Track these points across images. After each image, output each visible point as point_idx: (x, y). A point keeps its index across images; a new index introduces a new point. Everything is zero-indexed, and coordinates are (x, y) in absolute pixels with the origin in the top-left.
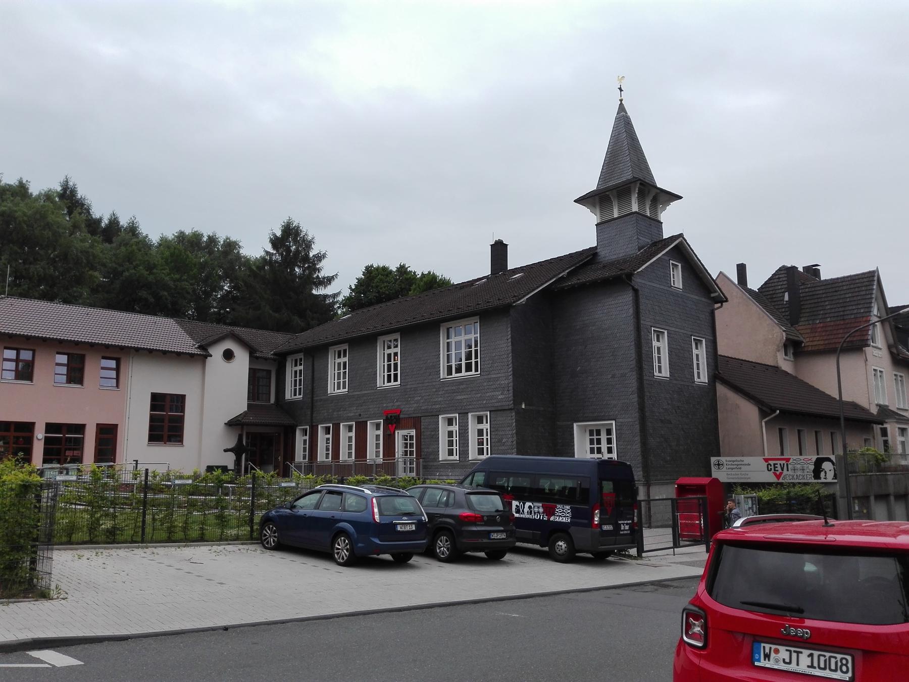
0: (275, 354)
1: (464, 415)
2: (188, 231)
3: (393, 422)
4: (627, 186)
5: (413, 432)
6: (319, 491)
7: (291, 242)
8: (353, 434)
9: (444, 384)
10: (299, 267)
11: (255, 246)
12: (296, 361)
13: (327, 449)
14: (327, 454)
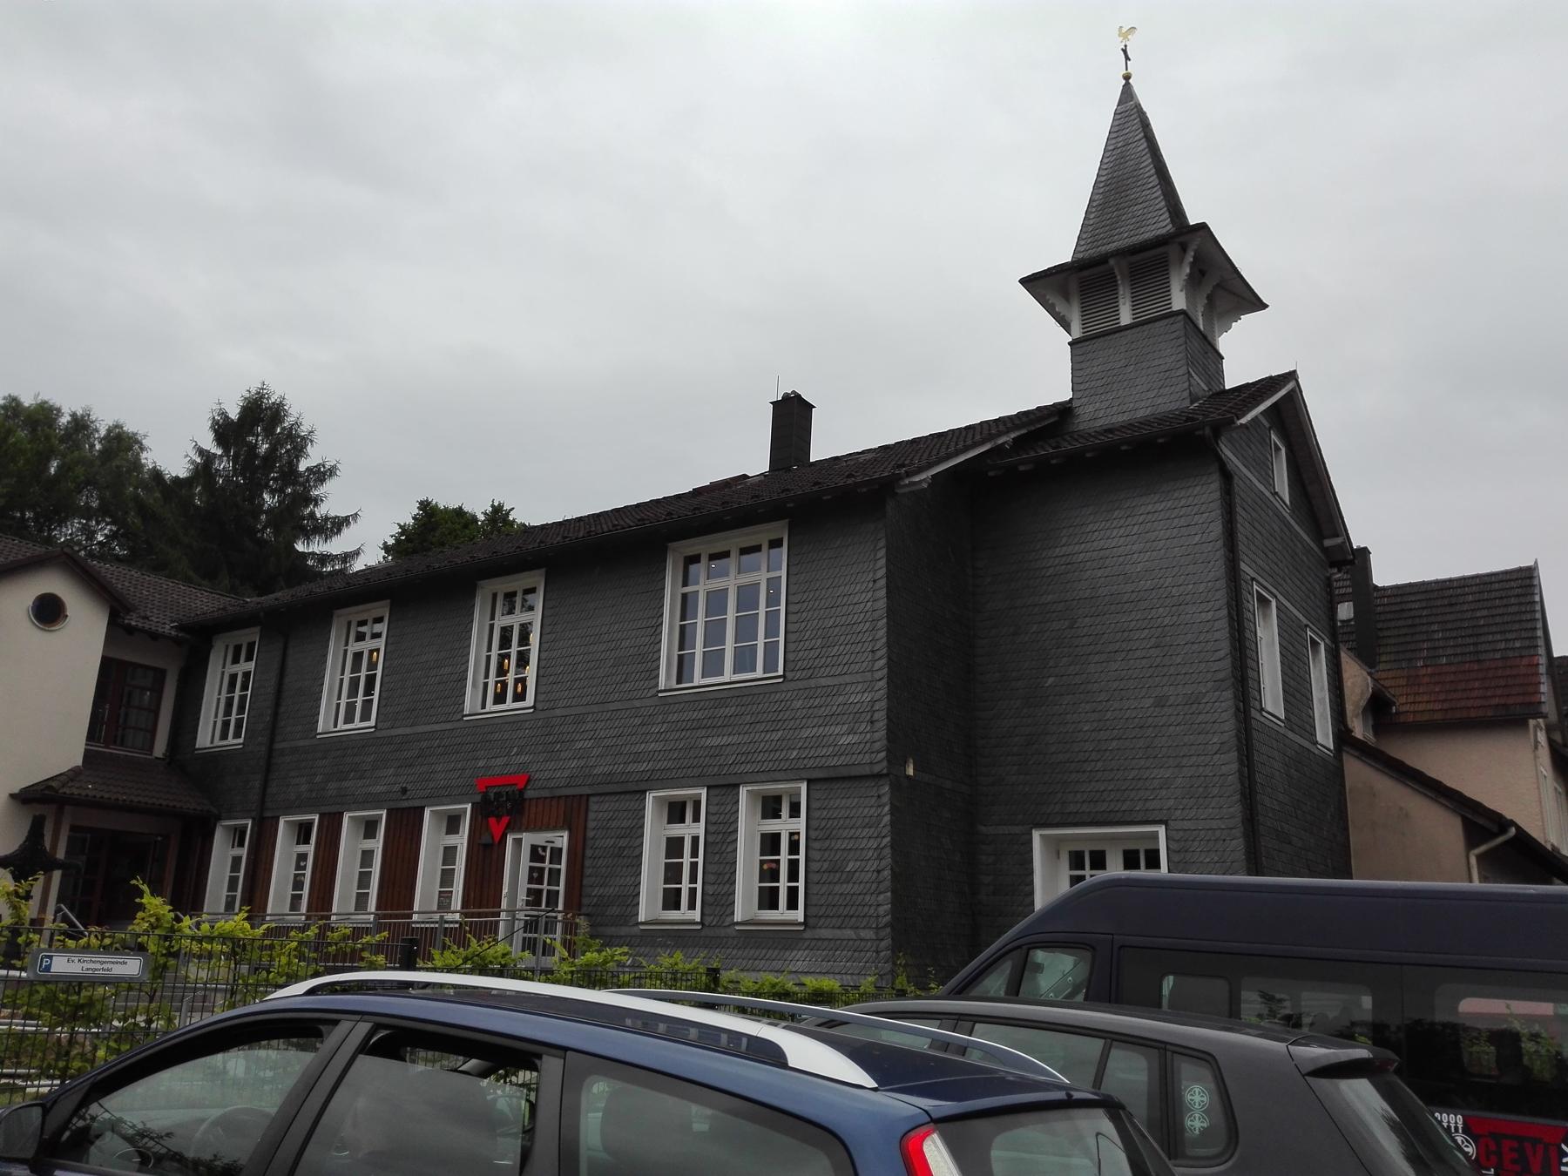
0: (181, 628)
1: (724, 790)
2: (27, 401)
3: (502, 809)
4: (1142, 259)
5: (562, 840)
6: (297, 1029)
7: (259, 437)
8: (377, 845)
9: (669, 703)
10: (273, 492)
11: (174, 447)
12: (238, 649)
13: (298, 885)
14: (296, 900)
